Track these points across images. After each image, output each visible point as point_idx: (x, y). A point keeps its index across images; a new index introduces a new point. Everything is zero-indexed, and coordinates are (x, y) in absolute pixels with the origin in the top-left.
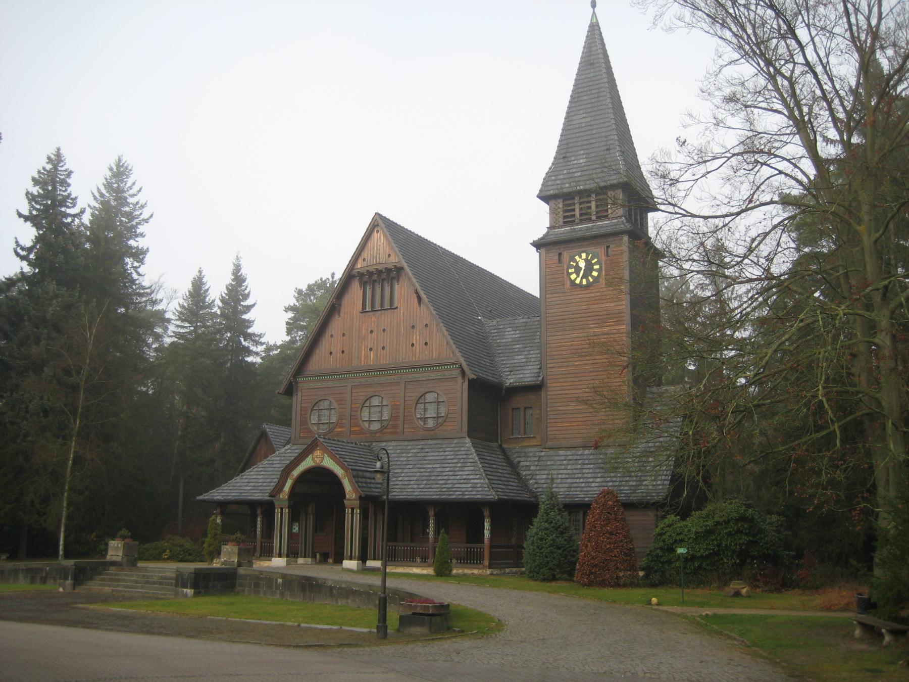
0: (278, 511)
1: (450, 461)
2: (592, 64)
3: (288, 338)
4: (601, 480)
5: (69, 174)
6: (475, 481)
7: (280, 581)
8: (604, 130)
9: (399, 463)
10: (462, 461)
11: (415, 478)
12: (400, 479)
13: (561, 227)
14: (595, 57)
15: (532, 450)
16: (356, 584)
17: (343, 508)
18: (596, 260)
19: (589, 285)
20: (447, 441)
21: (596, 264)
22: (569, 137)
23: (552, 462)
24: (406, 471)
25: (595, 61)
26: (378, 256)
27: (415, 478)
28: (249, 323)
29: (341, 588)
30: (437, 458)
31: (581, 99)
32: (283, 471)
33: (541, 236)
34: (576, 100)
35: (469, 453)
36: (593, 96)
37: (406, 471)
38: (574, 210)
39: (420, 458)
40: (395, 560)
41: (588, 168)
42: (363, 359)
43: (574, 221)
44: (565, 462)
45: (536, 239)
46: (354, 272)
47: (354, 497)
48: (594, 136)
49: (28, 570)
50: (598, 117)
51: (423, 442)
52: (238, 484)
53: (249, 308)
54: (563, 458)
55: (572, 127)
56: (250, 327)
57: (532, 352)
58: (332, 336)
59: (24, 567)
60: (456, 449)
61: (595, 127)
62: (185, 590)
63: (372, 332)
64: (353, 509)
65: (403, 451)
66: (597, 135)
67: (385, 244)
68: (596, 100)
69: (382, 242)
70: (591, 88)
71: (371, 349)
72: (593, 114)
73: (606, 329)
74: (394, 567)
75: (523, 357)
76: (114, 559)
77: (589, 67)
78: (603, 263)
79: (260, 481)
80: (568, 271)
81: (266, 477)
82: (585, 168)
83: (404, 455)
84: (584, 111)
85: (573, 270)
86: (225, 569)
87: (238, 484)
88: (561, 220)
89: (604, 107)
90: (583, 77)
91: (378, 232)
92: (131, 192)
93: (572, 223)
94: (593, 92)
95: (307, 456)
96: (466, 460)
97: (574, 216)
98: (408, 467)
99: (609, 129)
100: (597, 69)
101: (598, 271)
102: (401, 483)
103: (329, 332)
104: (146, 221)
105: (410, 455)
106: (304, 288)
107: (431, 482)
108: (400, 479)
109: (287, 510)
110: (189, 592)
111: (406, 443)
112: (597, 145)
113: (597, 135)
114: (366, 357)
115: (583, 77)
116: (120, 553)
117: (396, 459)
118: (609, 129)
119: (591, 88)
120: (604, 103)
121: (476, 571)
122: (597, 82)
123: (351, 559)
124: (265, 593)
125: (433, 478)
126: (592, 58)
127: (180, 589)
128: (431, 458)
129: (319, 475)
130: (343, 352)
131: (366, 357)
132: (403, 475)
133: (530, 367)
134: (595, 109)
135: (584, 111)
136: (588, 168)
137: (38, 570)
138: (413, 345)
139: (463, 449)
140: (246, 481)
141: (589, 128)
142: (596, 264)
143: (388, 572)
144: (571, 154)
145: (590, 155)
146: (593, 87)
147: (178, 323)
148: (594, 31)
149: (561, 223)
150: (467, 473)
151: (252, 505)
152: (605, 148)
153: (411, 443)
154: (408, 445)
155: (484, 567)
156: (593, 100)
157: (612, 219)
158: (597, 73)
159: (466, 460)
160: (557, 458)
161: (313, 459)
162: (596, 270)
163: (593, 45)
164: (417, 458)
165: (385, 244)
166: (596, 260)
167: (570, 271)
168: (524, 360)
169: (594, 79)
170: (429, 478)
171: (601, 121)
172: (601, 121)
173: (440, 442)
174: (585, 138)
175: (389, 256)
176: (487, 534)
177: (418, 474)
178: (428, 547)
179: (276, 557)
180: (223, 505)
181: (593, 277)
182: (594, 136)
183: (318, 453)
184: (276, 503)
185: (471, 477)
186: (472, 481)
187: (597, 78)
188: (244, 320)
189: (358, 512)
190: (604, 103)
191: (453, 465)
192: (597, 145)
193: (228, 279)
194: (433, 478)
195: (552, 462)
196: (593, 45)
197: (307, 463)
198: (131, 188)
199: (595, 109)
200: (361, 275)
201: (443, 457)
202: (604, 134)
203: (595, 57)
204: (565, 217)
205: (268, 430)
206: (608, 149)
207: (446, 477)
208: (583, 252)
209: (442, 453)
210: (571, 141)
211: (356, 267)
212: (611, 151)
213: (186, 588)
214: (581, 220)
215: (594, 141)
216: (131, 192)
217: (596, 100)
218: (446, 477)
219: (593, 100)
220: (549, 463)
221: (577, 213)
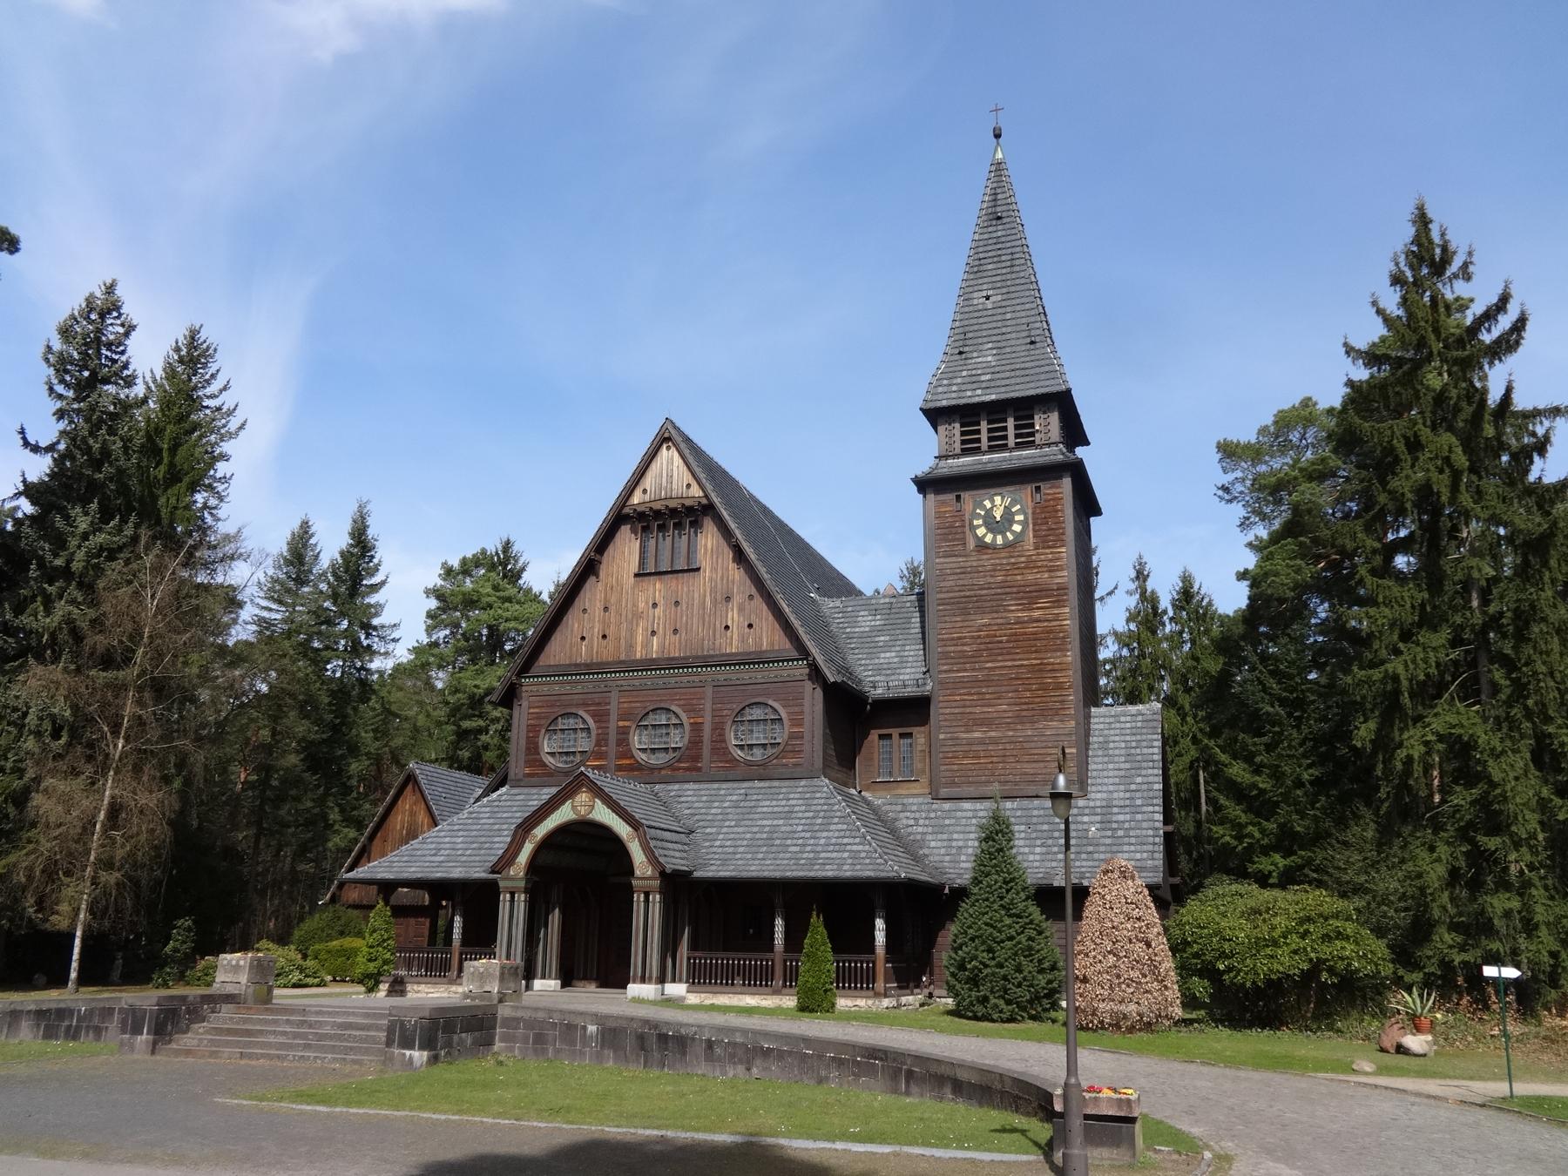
0: (505, 898)
1: (800, 815)
2: (999, 218)
3: (426, 641)
4: (1044, 850)
5: (130, 329)
6: (855, 848)
7: (592, 1029)
8: (1023, 314)
9: (710, 817)
10: (822, 814)
11: (745, 843)
12: (718, 843)
14: (1005, 208)
15: (915, 800)
16: (767, 1035)
17: (629, 890)
18: (1018, 507)
19: (1008, 546)
20: (787, 783)
21: (1018, 512)
22: (966, 323)
23: (953, 821)
24: (725, 830)
25: (1004, 214)
27: (745, 843)
28: (378, 609)
29: (733, 1044)
30: (776, 809)
31: (985, 268)
32: (519, 826)
33: (926, 469)
34: (976, 269)
35: (832, 801)
36: (1004, 265)
37: (725, 830)
39: (744, 810)
40: (733, 984)
41: (1003, 368)
42: (639, 649)
43: (979, 448)
45: (919, 473)
46: (626, 510)
48: (1009, 323)
49: (40, 1014)
50: (1013, 296)
51: (746, 784)
52: (419, 853)
53: (375, 588)
54: (970, 814)
55: (971, 309)
56: (377, 615)
57: (908, 648)
58: (585, 610)
59: (32, 1007)
60: (808, 795)
61: (1009, 309)
62: (408, 1053)
63: (655, 605)
64: (647, 895)
65: (713, 798)
66: (1014, 322)
68: (1008, 270)
69: (676, 464)
70: (999, 252)
71: (653, 633)
72: (1005, 290)
73: (1036, 614)
74: (711, 995)
75: (893, 654)
76: (230, 989)
79: (460, 846)
81: (469, 839)
82: (997, 369)
83: (716, 804)
84: (990, 286)
85: (980, 522)
86: (471, 1007)
87: (419, 853)
88: (958, 447)
89: (1023, 281)
90: (986, 236)
91: (668, 448)
92: (208, 391)
93: (977, 451)
94: (1003, 258)
95: (563, 803)
96: (828, 814)
98: (727, 823)
99: (1033, 312)
101: (1024, 523)
102: (720, 850)
103: (579, 603)
104: (232, 435)
105: (726, 804)
107: (774, 849)
108: (718, 843)
109: (523, 897)
110: (419, 1056)
111: (716, 786)
112: (1014, 335)
113: (1014, 322)
114: (647, 645)
115: (986, 236)
116: (243, 979)
117: (703, 811)
118: (1033, 312)
119: (999, 252)
120: (1022, 274)
121: (861, 1002)
122: (1009, 245)
123: (643, 980)
124: (558, 1051)
125: (778, 842)
126: (999, 209)
127: (397, 1051)
128: (765, 809)
129: (586, 834)
130: (604, 637)
131: (647, 645)
132: (721, 837)
133: (908, 670)
135: (990, 286)
136: (1003, 368)
137: (62, 1013)
138: (727, 627)
139: (818, 795)
140: (433, 846)
141: (1000, 311)
142: (1018, 512)
144: (971, 348)
145: (1004, 351)
146: (1004, 252)
147: (264, 603)
148: (998, 167)
149: (958, 451)
150: (837, 834)
151: (441, 889)
152: (1028, 340)
153: (724, 785)
154: (719, 789)
155: (877, 995)
156: (1004, 271)
157: (1041, 446)
158: (1009, 232)
159: (828, 814)
160: (959, 814)
161: (574, 807)
162: (1019, 522)
163: (999, 191)
164: (739, 810)
166: (1018, 507)
168: (896, 660)
169: (1003, 239)
170: (770, 842)
171: (1018, 301)
172: (1018, 301)
173: (776, 783)
174: (994, 325)
175: (689, 486)
176: (880, 937)
177: (748, 836)
178: (773, 961)
179: (634, 982)
180: (387, 888)
181: (1013, 532)
182: (1009, 323)
183: (583, 797)
184: (502, 884)
185: (846, 841)
186: (848, 847)
187: (1009, 238)
188: (369, 606)
190: (1022, 274)
191: (808, 821)
192: (1014, 335)
193: (343, 541)
194: (778, 842)
195: (953, 821)
196: (999, 191)
198: (208, 382)
201: (787, 809)
202: (1024, 320)
203: (1005, 208)
204: (963, 442)
205: (420, 777)
206: (1032, 343)
207: (800, 841)
208: (996, 494)
209: (784, 803)
210: (972, 328)
212: (1038, 345)
213: (411, 1047)
214: (990, 447)
215: (1009, 330)
216: (208, 391)
217: (1008, 270)
218: (800, 841)
219: (1004, 271)
220: (947, 822)
221: (984, 436)
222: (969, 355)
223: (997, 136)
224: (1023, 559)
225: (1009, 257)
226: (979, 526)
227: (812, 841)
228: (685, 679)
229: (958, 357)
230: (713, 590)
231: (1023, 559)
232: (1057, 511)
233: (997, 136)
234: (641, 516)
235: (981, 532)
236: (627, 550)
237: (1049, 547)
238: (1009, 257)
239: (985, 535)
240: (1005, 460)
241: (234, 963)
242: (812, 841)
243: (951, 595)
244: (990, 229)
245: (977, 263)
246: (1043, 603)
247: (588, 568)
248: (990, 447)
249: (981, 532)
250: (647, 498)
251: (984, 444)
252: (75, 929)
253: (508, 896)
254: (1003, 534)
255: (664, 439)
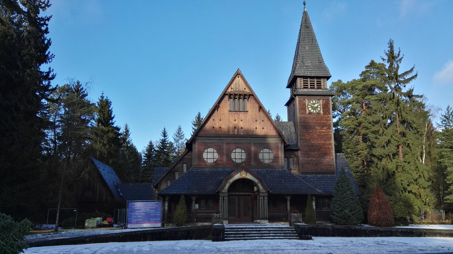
2: (308, 27)
13: (302, 89)
26: (239, 88)
38: (307, 83)
44: (129, 189)
46: (227, 93)
47: (264, 192)
67: (242, 84)
77: (306, 28)
78: (322, 105)
80: (308, 107)
90: (305, 31)
91: (238, 77)
94: (310, 38)
97: (307, 85)
100: (310, 30)
106: (367, 65)
119: (309, 37)
134: (312, 45)
143: (159, 223)
148: (305, 13)
149: (303, 88)
157: (324, 89)
163: (307, 20)
165: (242, 84)
167: (309, 107)
175: (245, 89)
189: (267, 198)
197: (237, 176)
199: (312, 45)
200: (230, 95)
211: (228, 91)
221: (309, 84)
222: (304, 63)
223: (304, 4)
224: (320, 117)
225: (311, 38)
226: (310, 108)
227: (213, 181)
228: (246, 141)
229: (301, 63)
230: (252, 118)
231: (320, 117)
232: (328, 106)
233: (304, 4)
234: (230, 95)
235: (310, 109)
236: (227, 104)
237: (327, 115)
238: (311, 38)
239: (311, 110)
240: (315, 91)
241: (218, 216)
242: (213, 181)
243: (303, 124)
244: (306, 30)
245: (303, 38)
246: (325, 128)
247: (216, 107)
248: (317, 88)
249: (310, 109)
250: (233, 90)
251: (309, 87)
252: (290, 209)
253: (222, 198)
254: (315, 110)
255: (238, 74)
